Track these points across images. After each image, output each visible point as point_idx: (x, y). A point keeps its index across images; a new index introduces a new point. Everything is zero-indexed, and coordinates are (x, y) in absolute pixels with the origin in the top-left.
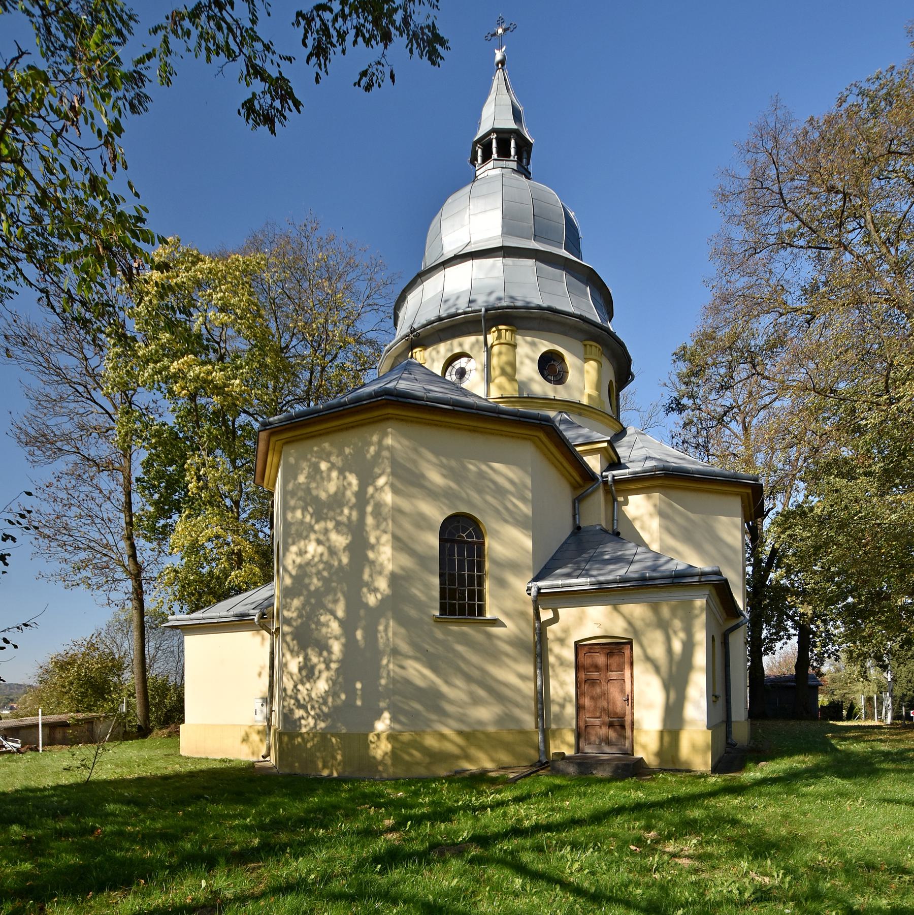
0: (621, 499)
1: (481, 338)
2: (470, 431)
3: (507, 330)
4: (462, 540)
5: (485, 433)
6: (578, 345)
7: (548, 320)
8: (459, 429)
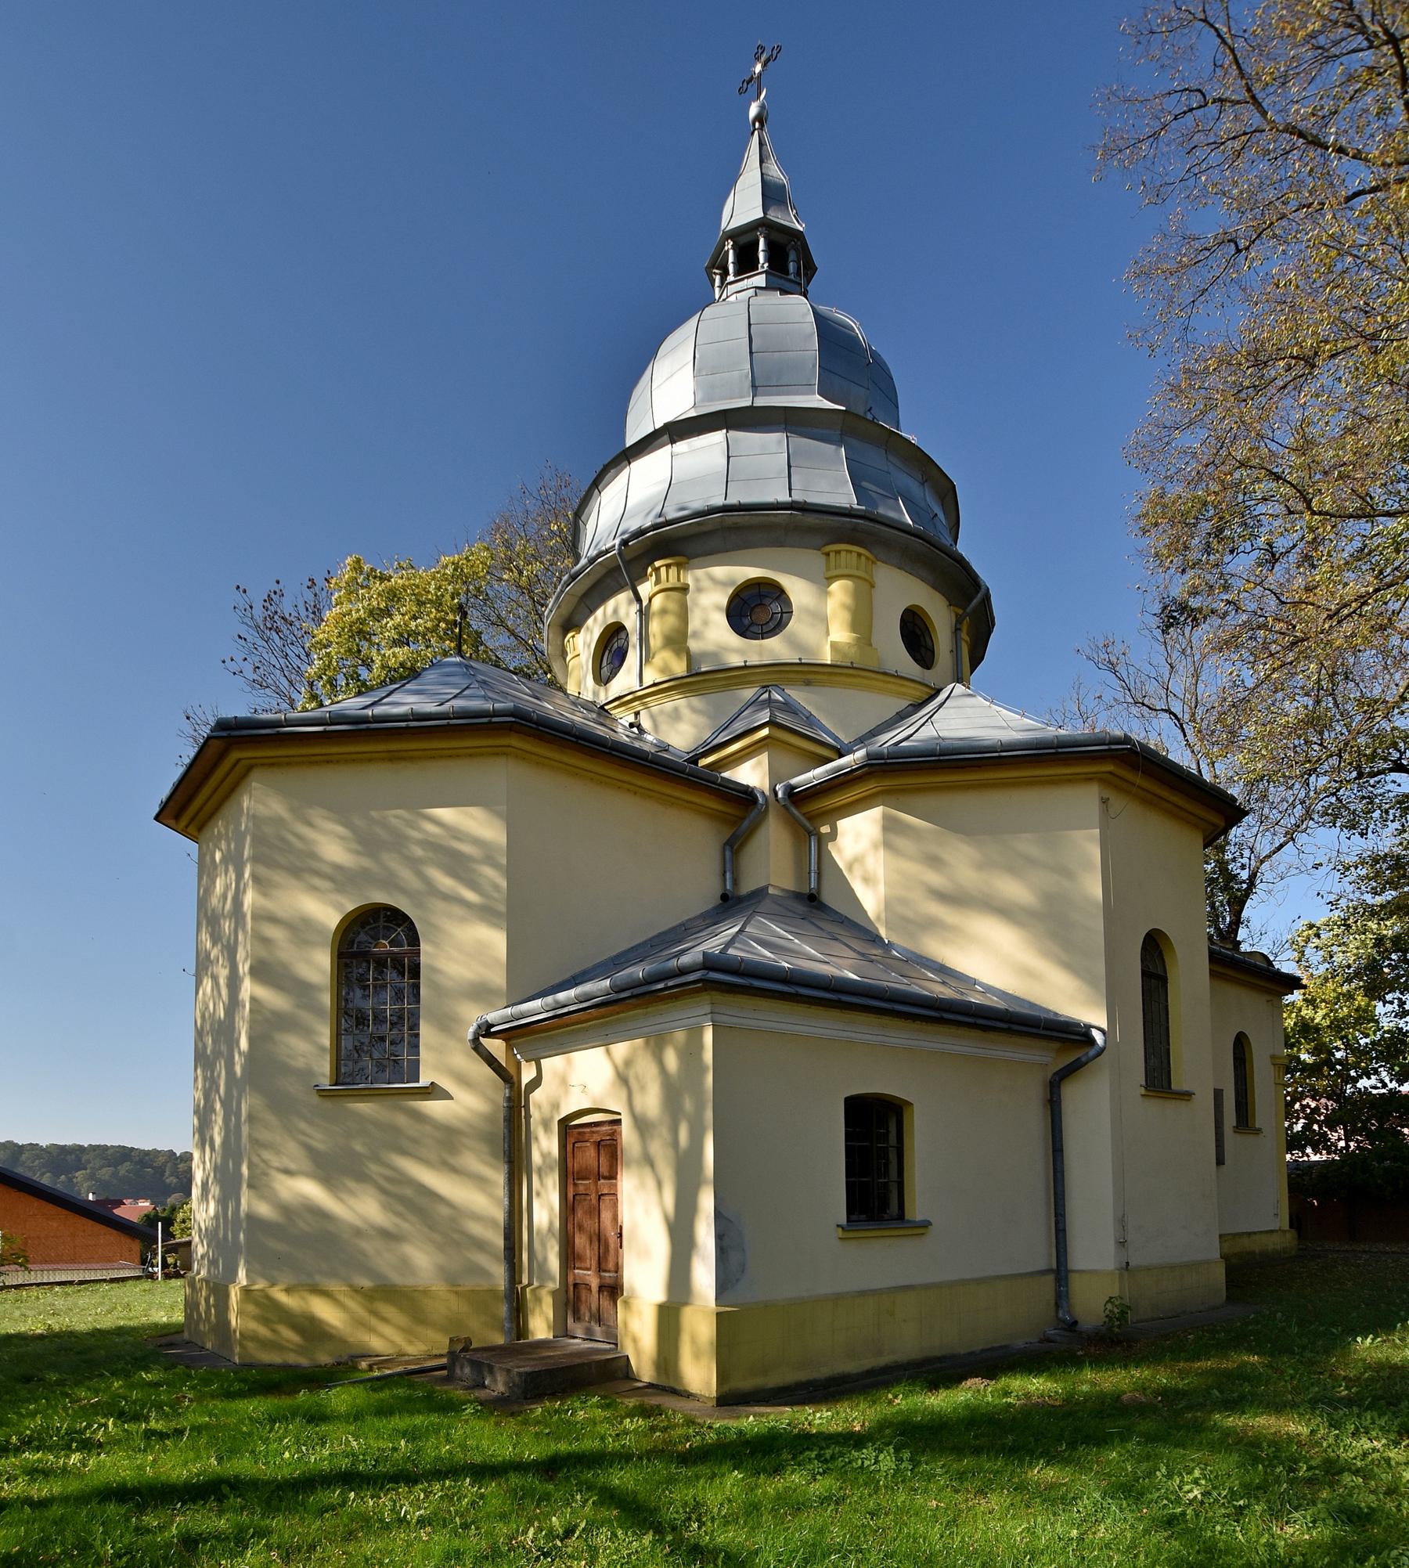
0: (825, 829)
1: (629, 594)
2: (390, 760)
3: (668, 566)
4: (378, 952)
5: (420, 758)
6: (812, 558)
7: (736, 528)
8: (370, 760)
